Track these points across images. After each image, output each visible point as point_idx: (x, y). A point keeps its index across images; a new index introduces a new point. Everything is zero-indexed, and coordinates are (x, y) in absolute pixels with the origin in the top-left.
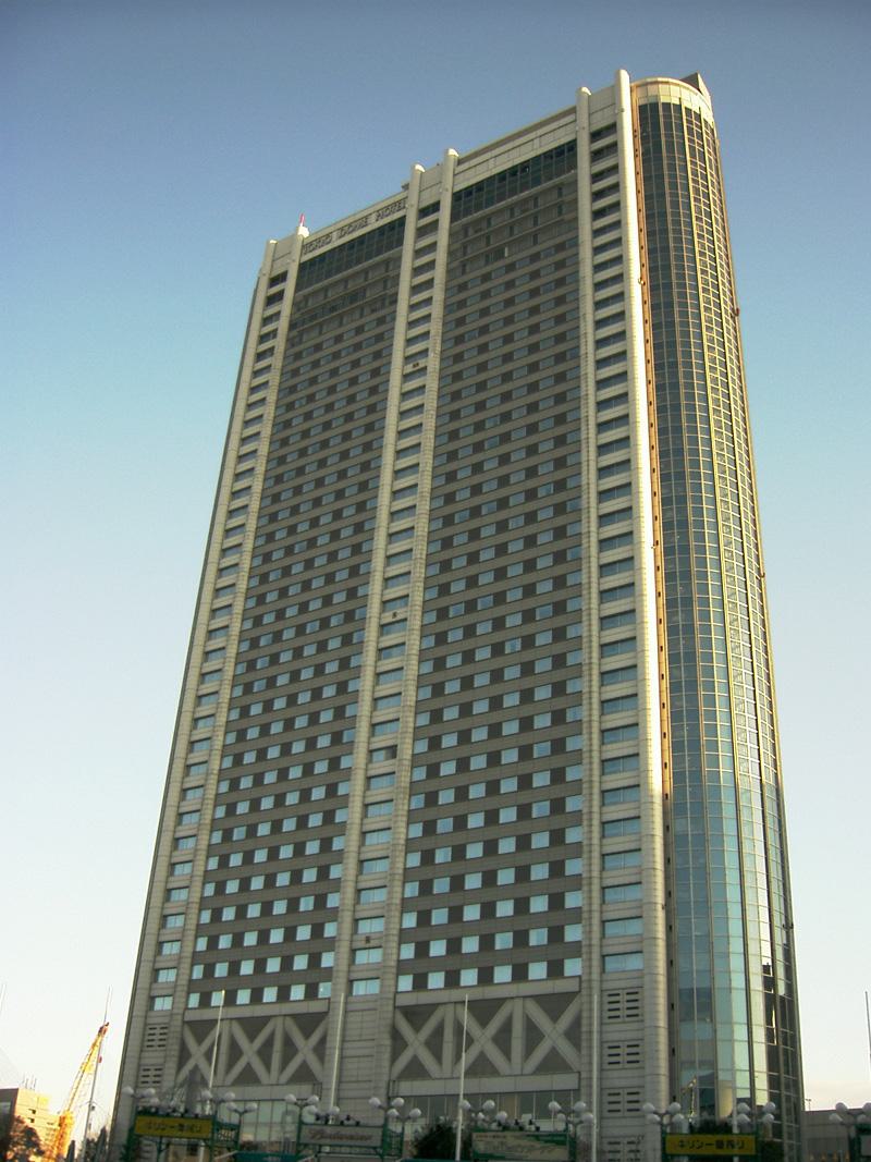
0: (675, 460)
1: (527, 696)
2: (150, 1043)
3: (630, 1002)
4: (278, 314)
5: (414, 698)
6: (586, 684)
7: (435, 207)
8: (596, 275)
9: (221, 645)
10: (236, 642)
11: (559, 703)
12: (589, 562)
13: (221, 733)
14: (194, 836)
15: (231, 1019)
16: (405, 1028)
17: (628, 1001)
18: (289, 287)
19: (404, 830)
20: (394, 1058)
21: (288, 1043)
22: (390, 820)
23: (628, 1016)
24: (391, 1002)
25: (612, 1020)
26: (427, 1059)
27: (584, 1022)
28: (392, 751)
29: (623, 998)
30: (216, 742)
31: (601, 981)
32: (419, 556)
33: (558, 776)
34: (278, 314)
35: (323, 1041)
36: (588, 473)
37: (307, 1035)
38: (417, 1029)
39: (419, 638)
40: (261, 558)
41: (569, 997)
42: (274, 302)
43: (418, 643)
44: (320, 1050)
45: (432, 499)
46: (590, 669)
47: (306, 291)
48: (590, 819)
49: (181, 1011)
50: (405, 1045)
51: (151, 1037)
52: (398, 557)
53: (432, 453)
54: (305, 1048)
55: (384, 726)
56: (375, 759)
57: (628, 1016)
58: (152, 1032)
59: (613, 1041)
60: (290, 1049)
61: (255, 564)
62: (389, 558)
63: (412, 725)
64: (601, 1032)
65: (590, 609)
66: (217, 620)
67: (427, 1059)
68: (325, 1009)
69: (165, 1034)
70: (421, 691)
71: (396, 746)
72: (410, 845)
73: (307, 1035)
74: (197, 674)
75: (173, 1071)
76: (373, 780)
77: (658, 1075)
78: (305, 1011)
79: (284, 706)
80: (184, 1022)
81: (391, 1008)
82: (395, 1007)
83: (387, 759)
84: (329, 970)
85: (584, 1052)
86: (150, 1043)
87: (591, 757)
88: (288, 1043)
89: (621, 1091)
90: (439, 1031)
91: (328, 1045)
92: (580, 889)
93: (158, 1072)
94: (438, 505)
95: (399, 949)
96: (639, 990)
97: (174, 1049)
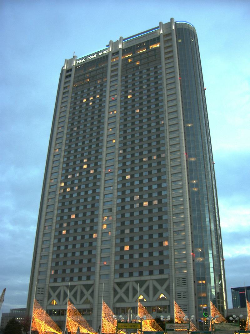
0: (196, 196)
1: (149, 125)
2: (38, 293)
3: (183, 281)
4: (70, 81)
5: (116, 195)
6: (167, 177)
7: (117, 64)
8: (166, 56)
9: (61, 142)
10: (61, 177)
11: (159, 174)
12: (170, 205)
13: (57, 203)
14: (56, 185)
15: (64, 286)
16: (118, 288)
17: (183, 283)
18: (73, 73)
19: (116, 201)
20: (115, 296)
21: (82, 293)
22: (112, 206)
23: (184, 297)
24: (113, 281)
25: (178, 299)
26: (124, 297)
27: (171, 286)
28: (111, 210)
29: (181, 280)
30: (56, 206)
31: (175, 275)
32: (116, 154)
33: (159, 186)
34: (70, 81)
35: (93, 292)
36: (167, 133)
37: (88, 290)
38: (121, 288)
39: (117, 178)
40: (68, 141)
41: (166, 280)
42: (68, 77)
43: (117, 179)
44: (92, 294)
45: (119, 138)
46: (169, 188)
47: (78, 75)
48: (171, 230)
49: (48, 284)
50: (118, 293)
51: (39, 291)
52: (112, 107)
53: (119, 125)
54: (87, 294)
55: (109, 181)
56: (106, 176)
57: (184, 297)
58: (39, 289)
59: (178, 278)
60: (82, 294)
61: (70, 115)
62: (111, 82)
63: (116, 202)
64: (175, 289)
65: (171, 229)
66: (58, 136)
67: (124, 297)
68: (93, 283)
69: (43, 292)
70: (118, 193)
71: (112, 208)
72: (118, 197)
73: (88, 290)
74: (48, 186)
75: (46, 301)
76: (103, 234)
77: (192, 301)
78: (87, 284)
79: (79, 169)
80: (49, 287)
81: (113, 283)
82: (114, 282)
83: (109, 212)
84: (96, 238)
85: (171, 295)
86: (38, 293)
87: (170, 213)
88: (82, 293)
89: (181, 292)
90: (128, 289)
91: (94, 293)
92: (167, 215)
93: (41, 301)
94: (123, 89)
95: (117, 200)
96: (186, 278)
97: (47, 295)
